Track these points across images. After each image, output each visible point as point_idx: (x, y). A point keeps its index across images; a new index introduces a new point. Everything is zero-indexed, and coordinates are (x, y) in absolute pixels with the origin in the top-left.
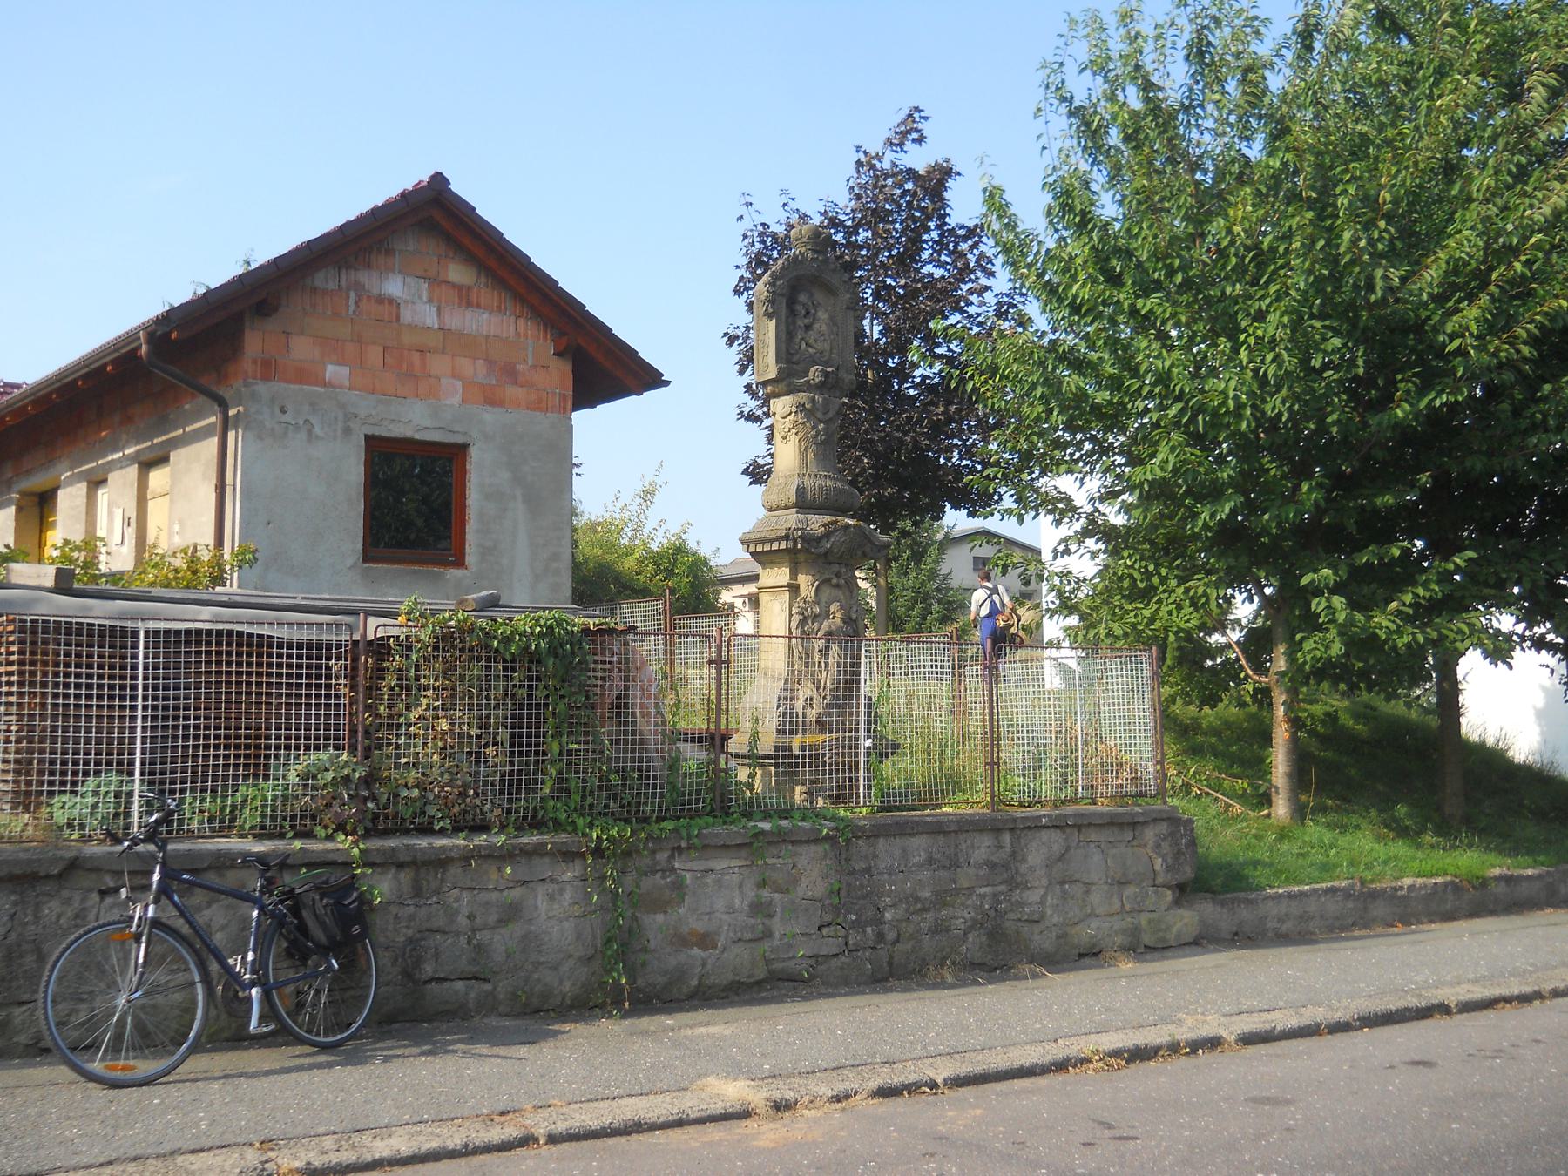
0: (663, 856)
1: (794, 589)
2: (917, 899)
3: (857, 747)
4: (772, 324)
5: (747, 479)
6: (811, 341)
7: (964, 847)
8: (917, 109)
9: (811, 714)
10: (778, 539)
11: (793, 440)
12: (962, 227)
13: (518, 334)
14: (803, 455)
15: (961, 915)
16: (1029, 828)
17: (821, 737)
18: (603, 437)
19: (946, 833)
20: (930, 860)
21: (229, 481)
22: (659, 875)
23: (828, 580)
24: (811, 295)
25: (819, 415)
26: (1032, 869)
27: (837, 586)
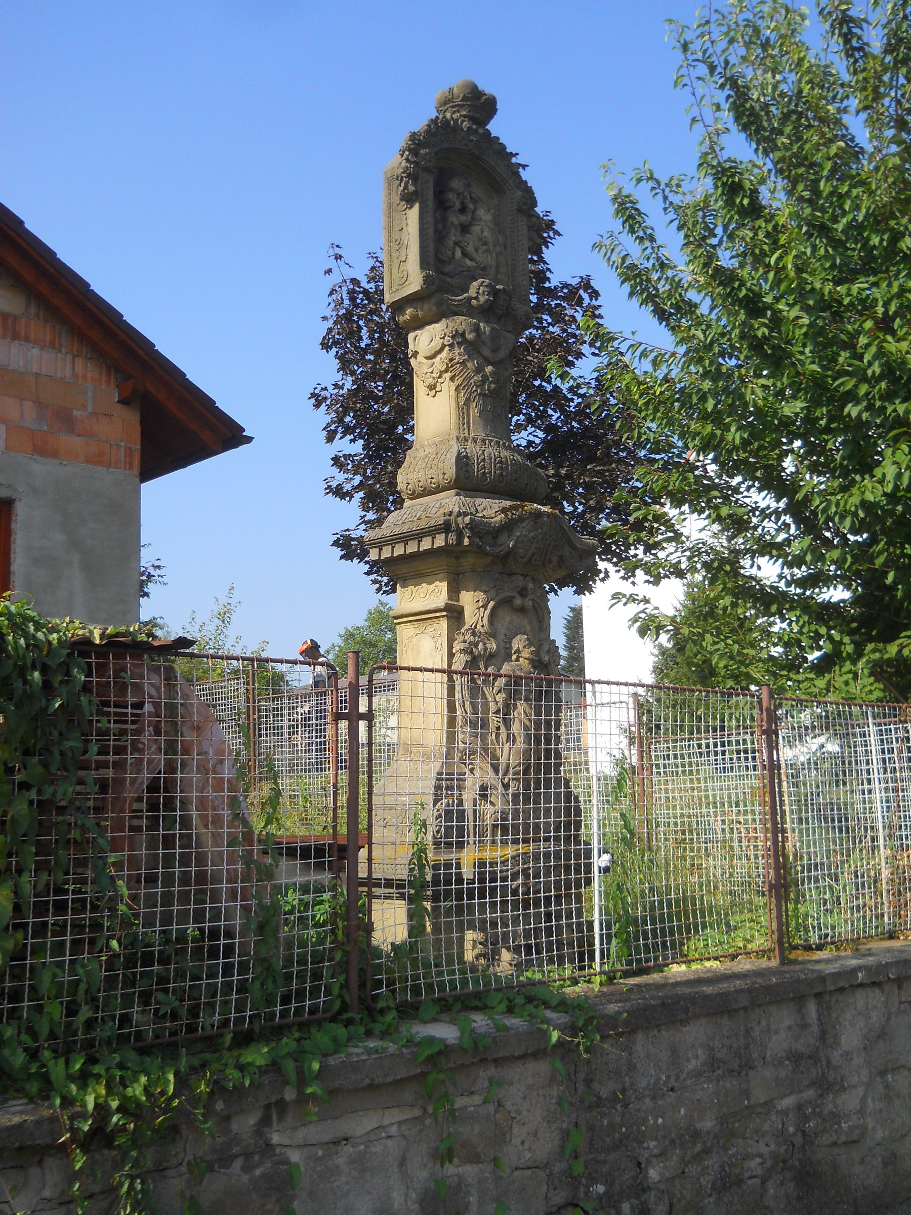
0: (245, 1124)
1: (454, 614)
2: (696, 1135)
3: (589, 868)
4: (414, 214)
5: (339, 552)
6: (470, 248)
7: (756, 1032)
9: (490, 812)
10: (431, 532)
11: (447, 388)
12: (565, 285)
13: (75, 375)
14: (463, 410)
15: (757, 1151)
16: (842, 990)
17: (510, 851)
18: (174, 507)
19: (731, 1013)
20: (712, 1063)
22: (238, 1164)
24: (469, 185)
25: (486, 352)
26: (847, 1056)
27: (522, 610)
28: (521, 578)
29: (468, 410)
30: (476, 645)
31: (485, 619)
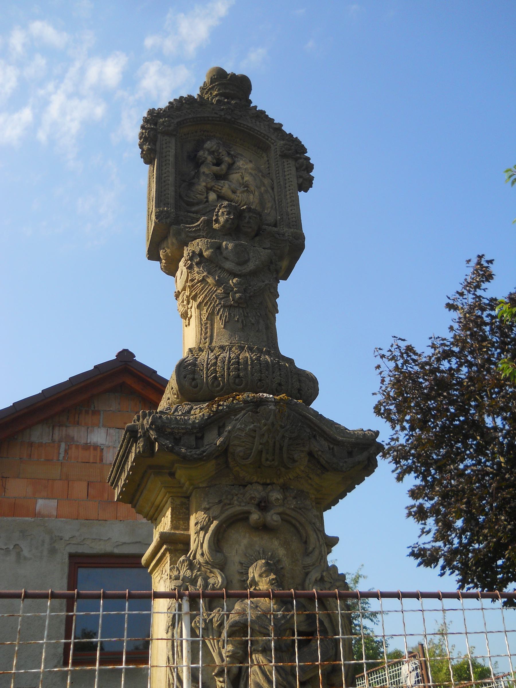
8: (480, 257)
21: (179, 648)
23: (242, 518)
27: (264, 528)
28: (260, 488)
29: (212, 325)
30: (193, 582)
31: (205, 546)
